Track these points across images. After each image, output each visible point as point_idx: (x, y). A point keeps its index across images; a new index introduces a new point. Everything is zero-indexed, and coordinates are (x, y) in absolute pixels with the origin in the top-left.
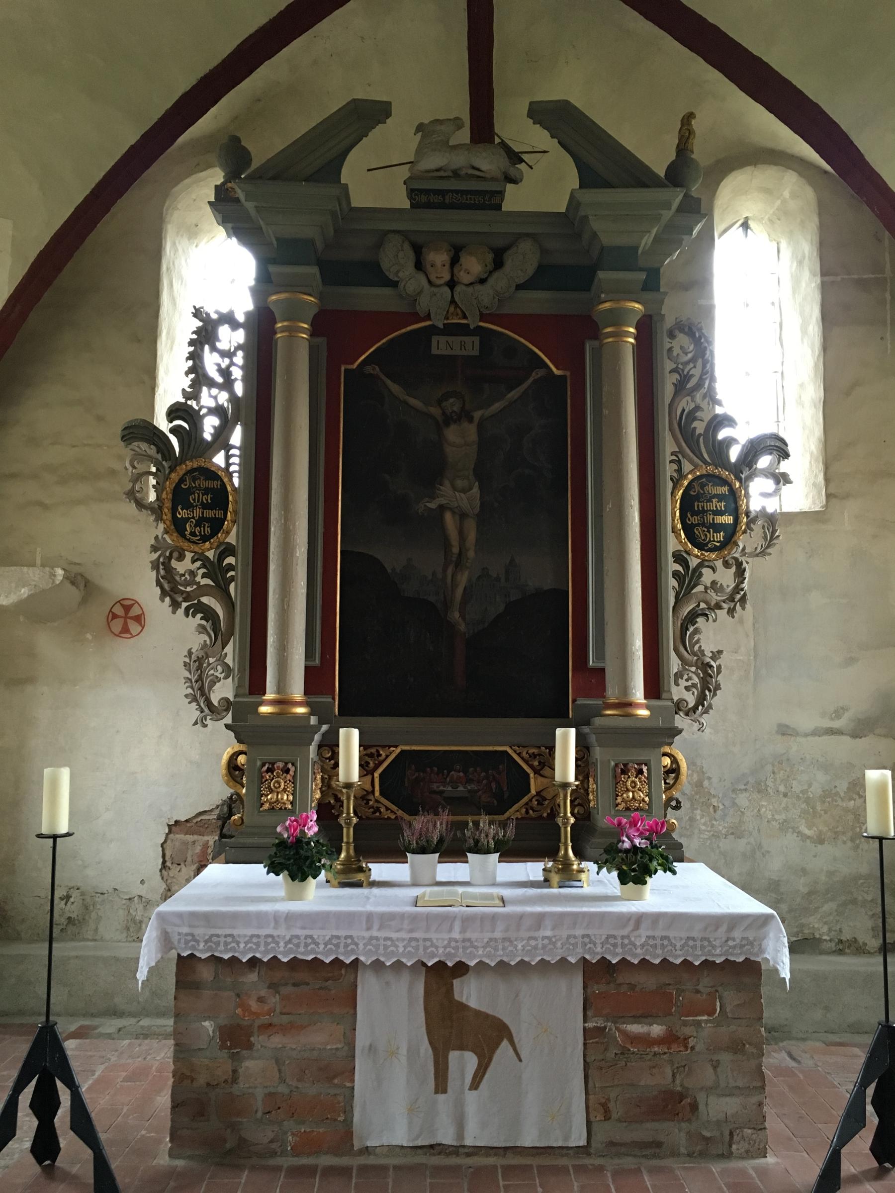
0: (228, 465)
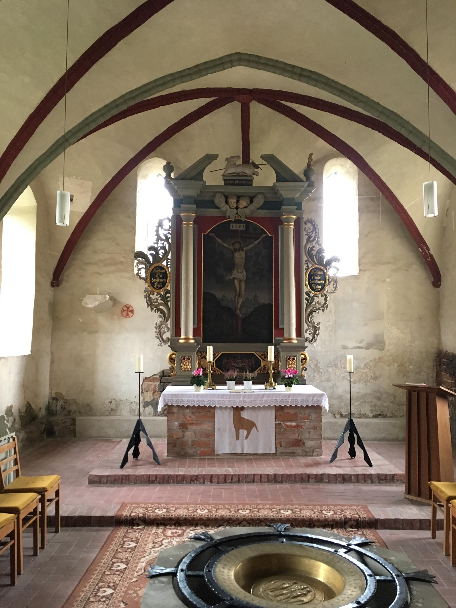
0: (167, 265)
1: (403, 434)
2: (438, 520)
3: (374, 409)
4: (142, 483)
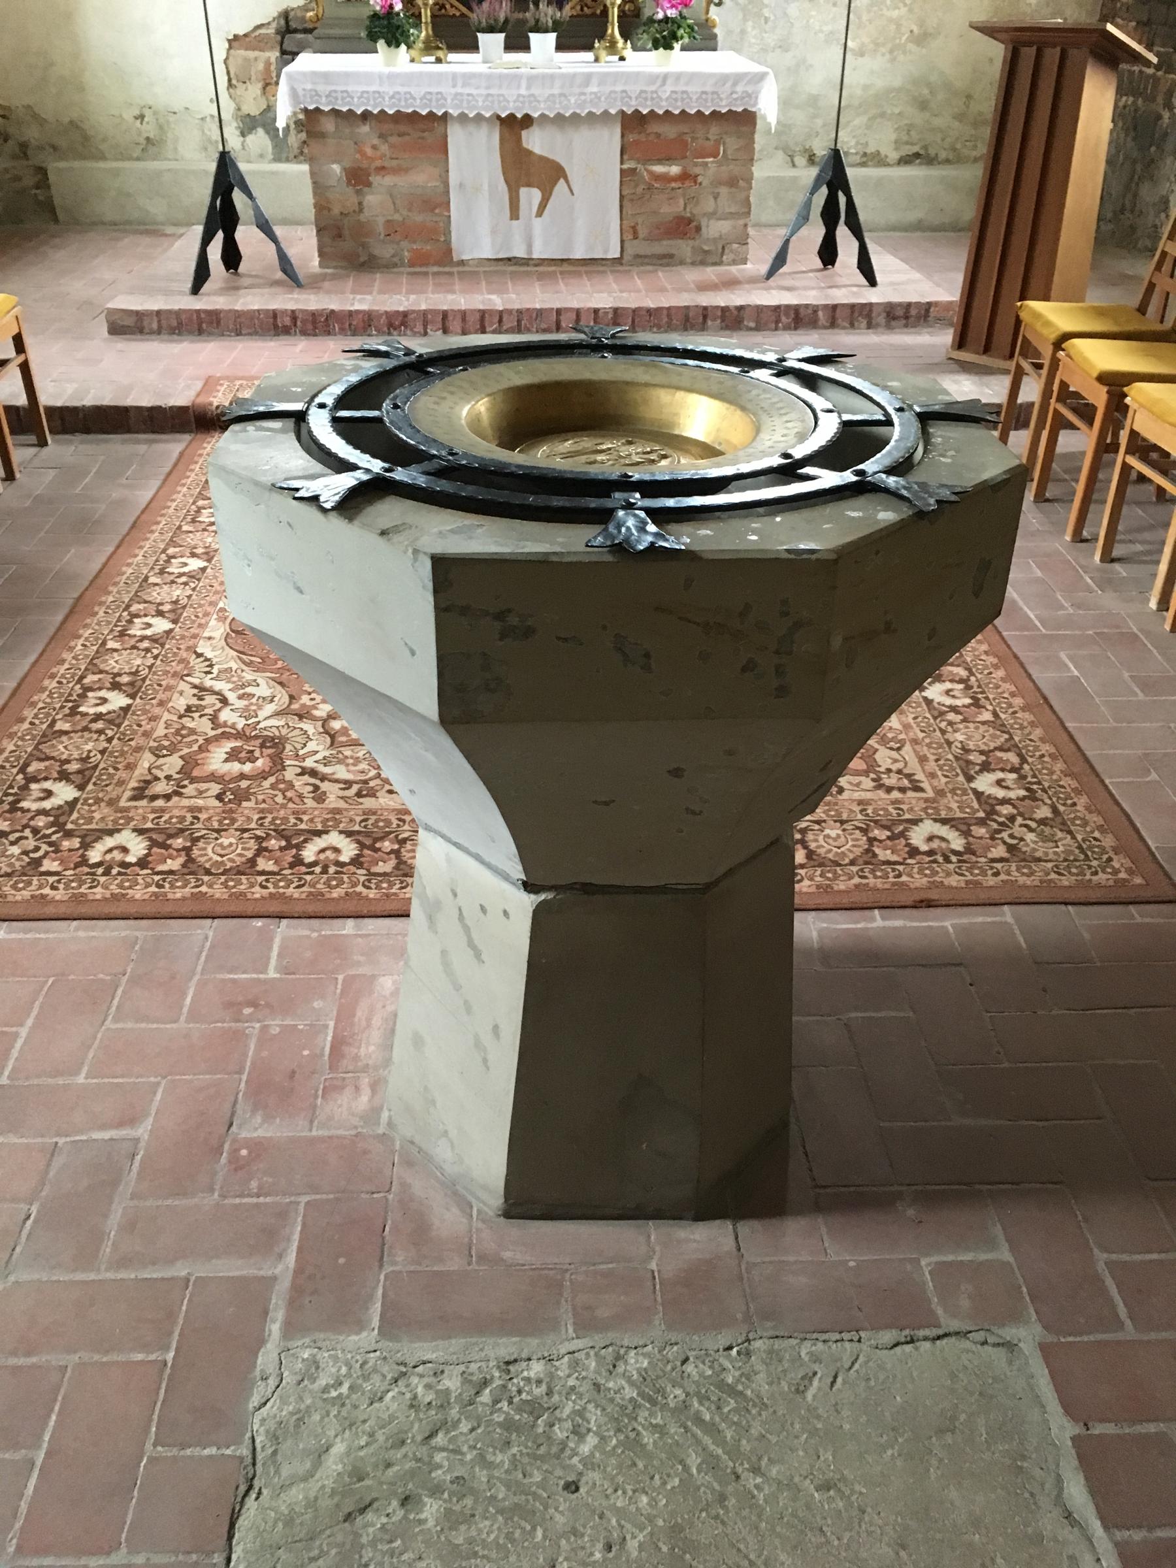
1: (969, 212)
2: (1021, 405)
3: (905, 138)
4: (255, 333)
